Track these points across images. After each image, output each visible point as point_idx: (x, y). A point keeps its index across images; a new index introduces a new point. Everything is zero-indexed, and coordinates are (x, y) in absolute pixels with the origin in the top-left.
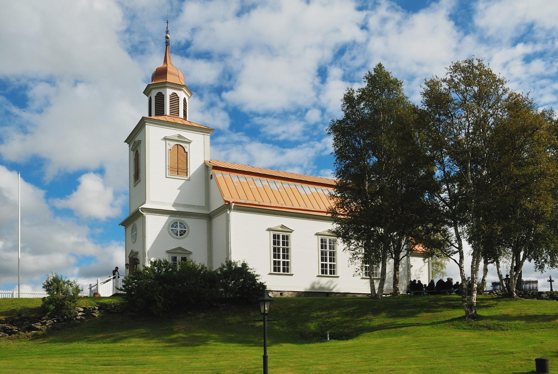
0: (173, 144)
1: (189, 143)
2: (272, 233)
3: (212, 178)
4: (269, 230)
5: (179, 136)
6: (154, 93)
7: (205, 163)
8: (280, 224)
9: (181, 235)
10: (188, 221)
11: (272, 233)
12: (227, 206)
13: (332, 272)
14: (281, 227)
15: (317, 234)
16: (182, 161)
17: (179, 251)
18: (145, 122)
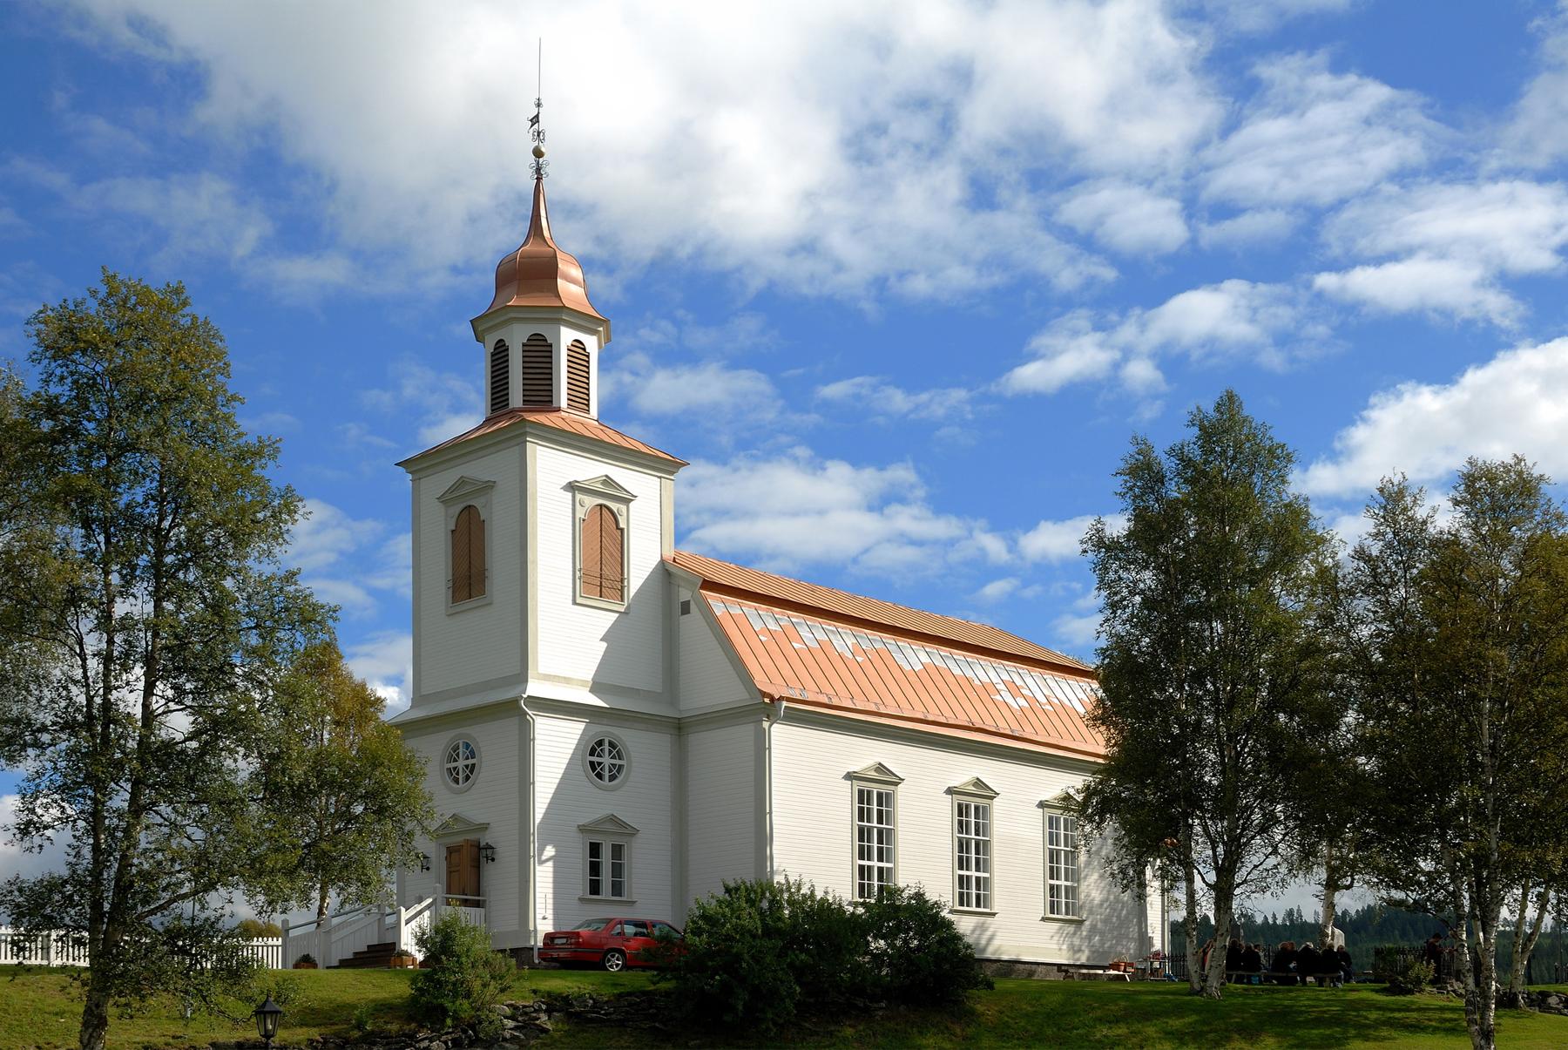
0: (591, 501)
4: (850, 776)
5: (608, 481)
6: (517, 338)
7: (663, 562)
9: (612, 778)
10: (628, 737)
11: (857, 785)
12: (767, 707)
14: (975, 785)
15: (950, 791)
16: (611, 555)
18: (525, 434)
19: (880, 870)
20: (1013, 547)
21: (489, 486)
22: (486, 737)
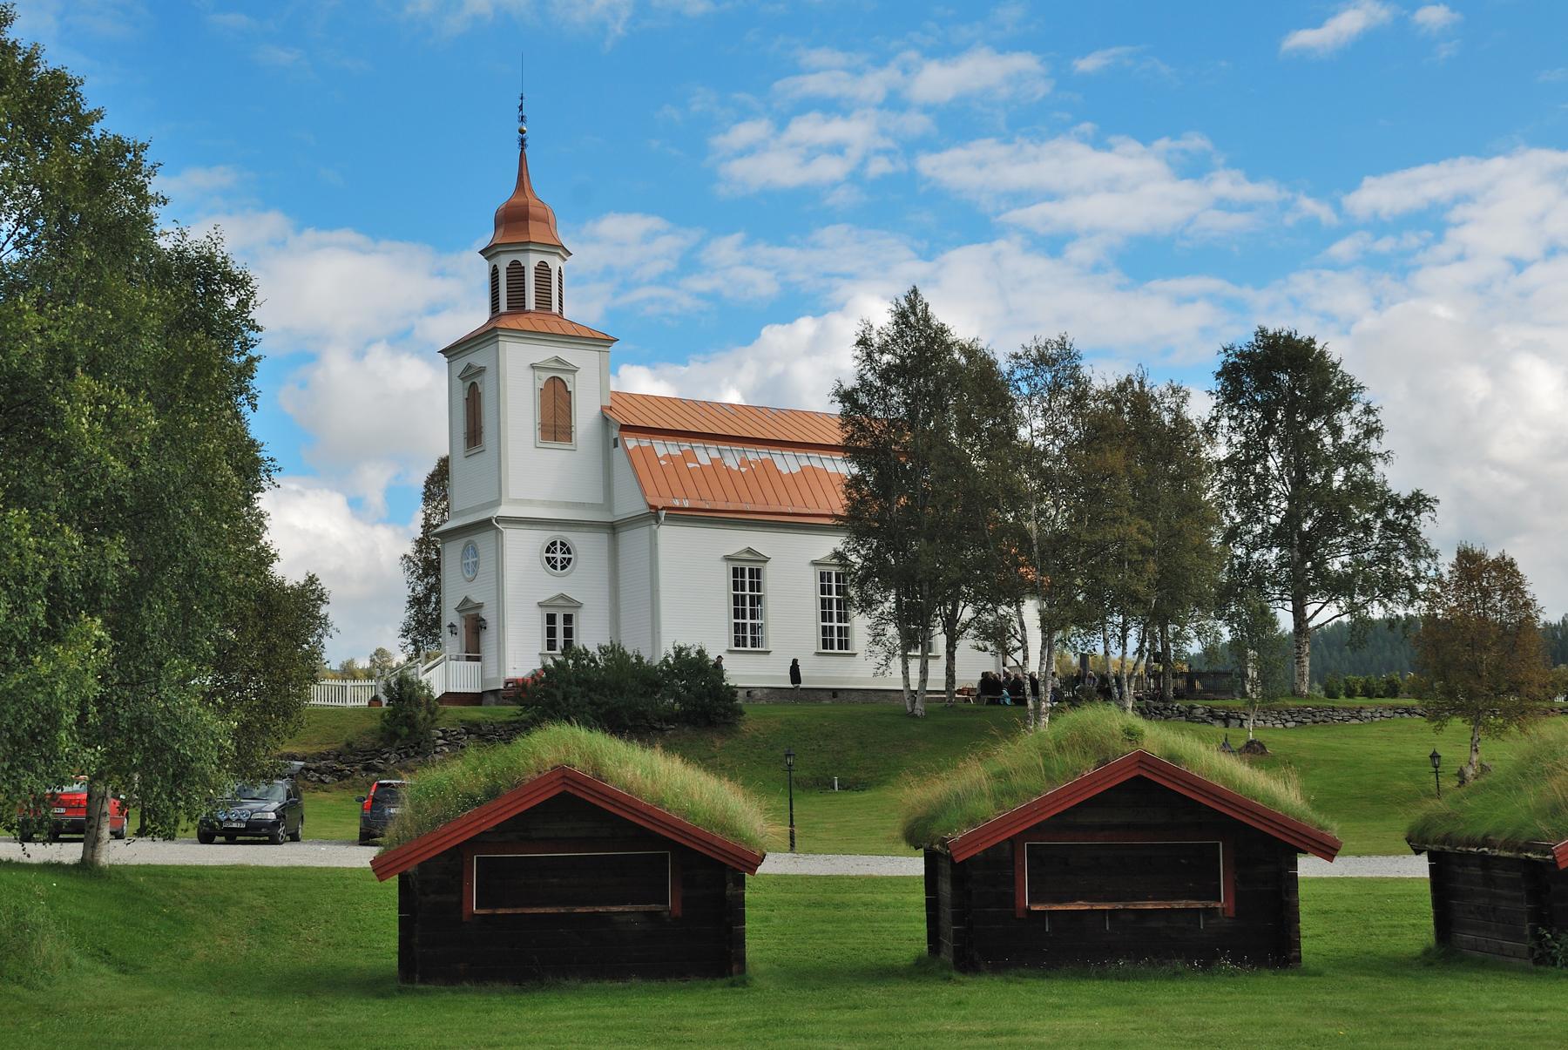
1: (574, 371)
2: (731, 565)
3: (616, 446)
4: (728, 558)
5: (558, 360)
6: (504, 262)
8: (744, 547)
9: (563, 568)
10: (572, 537)
13: (844, 644)
17: (560, 602)
19: (753, 626)
20: (1338, 207)
21: (482, 370)
22: (483, 540)
